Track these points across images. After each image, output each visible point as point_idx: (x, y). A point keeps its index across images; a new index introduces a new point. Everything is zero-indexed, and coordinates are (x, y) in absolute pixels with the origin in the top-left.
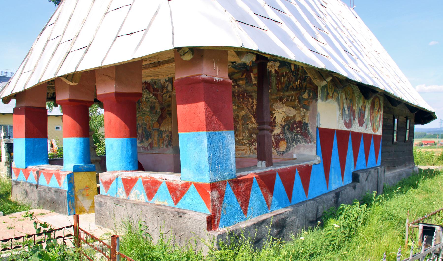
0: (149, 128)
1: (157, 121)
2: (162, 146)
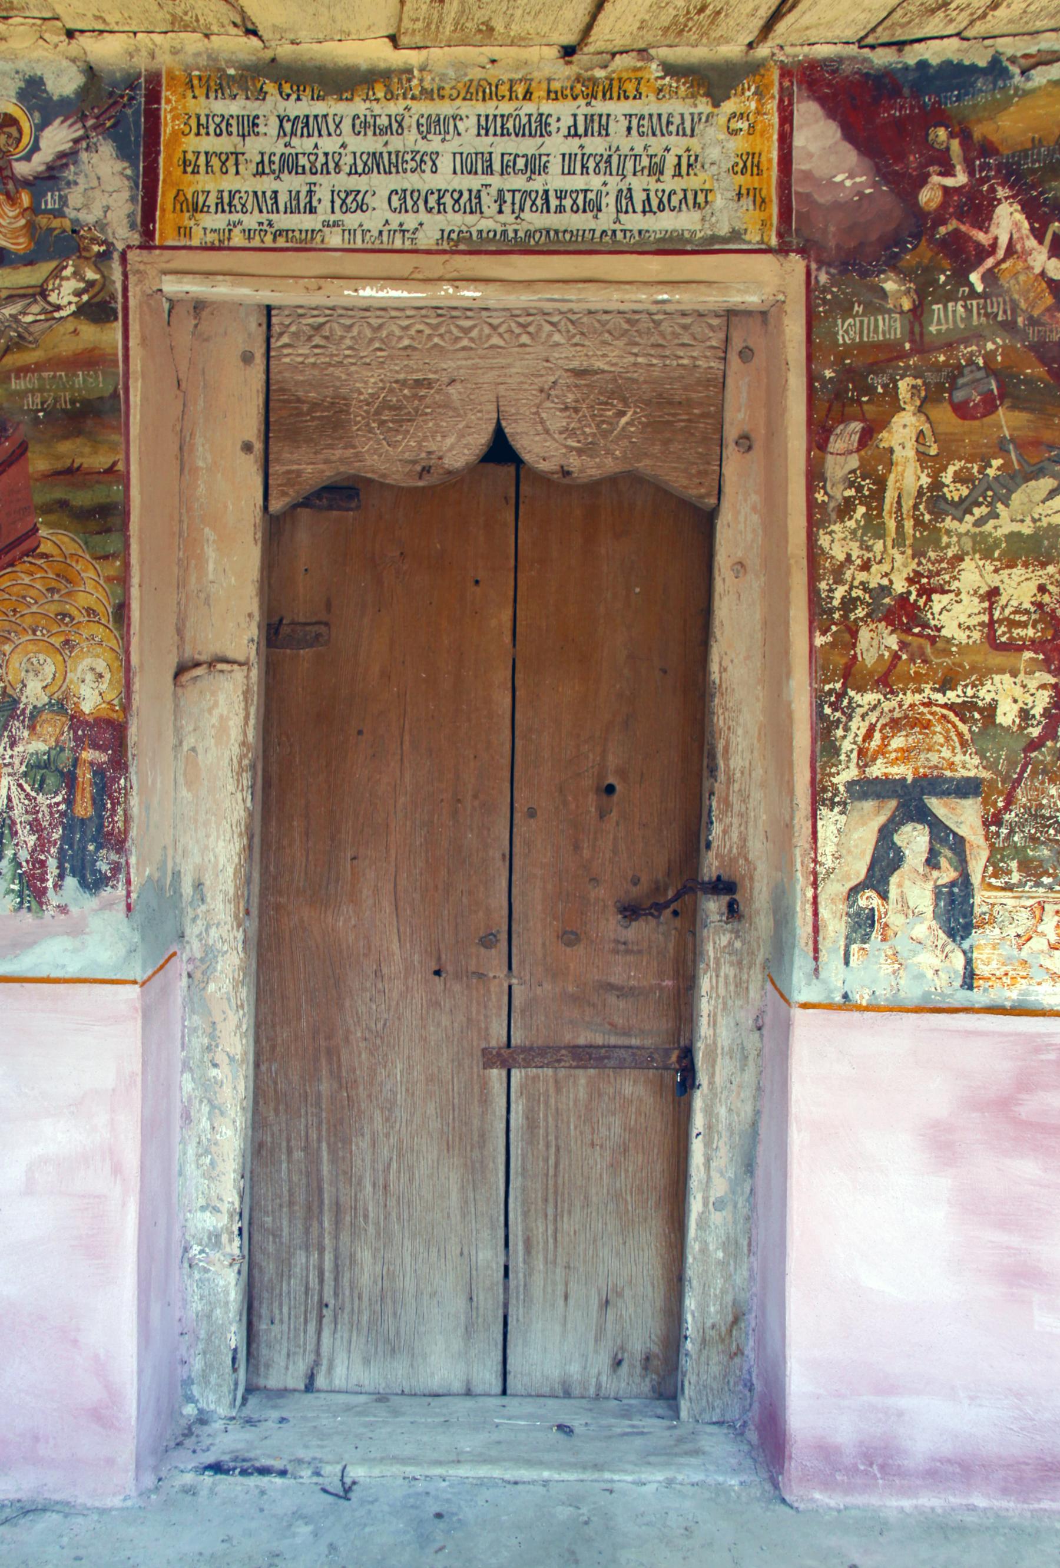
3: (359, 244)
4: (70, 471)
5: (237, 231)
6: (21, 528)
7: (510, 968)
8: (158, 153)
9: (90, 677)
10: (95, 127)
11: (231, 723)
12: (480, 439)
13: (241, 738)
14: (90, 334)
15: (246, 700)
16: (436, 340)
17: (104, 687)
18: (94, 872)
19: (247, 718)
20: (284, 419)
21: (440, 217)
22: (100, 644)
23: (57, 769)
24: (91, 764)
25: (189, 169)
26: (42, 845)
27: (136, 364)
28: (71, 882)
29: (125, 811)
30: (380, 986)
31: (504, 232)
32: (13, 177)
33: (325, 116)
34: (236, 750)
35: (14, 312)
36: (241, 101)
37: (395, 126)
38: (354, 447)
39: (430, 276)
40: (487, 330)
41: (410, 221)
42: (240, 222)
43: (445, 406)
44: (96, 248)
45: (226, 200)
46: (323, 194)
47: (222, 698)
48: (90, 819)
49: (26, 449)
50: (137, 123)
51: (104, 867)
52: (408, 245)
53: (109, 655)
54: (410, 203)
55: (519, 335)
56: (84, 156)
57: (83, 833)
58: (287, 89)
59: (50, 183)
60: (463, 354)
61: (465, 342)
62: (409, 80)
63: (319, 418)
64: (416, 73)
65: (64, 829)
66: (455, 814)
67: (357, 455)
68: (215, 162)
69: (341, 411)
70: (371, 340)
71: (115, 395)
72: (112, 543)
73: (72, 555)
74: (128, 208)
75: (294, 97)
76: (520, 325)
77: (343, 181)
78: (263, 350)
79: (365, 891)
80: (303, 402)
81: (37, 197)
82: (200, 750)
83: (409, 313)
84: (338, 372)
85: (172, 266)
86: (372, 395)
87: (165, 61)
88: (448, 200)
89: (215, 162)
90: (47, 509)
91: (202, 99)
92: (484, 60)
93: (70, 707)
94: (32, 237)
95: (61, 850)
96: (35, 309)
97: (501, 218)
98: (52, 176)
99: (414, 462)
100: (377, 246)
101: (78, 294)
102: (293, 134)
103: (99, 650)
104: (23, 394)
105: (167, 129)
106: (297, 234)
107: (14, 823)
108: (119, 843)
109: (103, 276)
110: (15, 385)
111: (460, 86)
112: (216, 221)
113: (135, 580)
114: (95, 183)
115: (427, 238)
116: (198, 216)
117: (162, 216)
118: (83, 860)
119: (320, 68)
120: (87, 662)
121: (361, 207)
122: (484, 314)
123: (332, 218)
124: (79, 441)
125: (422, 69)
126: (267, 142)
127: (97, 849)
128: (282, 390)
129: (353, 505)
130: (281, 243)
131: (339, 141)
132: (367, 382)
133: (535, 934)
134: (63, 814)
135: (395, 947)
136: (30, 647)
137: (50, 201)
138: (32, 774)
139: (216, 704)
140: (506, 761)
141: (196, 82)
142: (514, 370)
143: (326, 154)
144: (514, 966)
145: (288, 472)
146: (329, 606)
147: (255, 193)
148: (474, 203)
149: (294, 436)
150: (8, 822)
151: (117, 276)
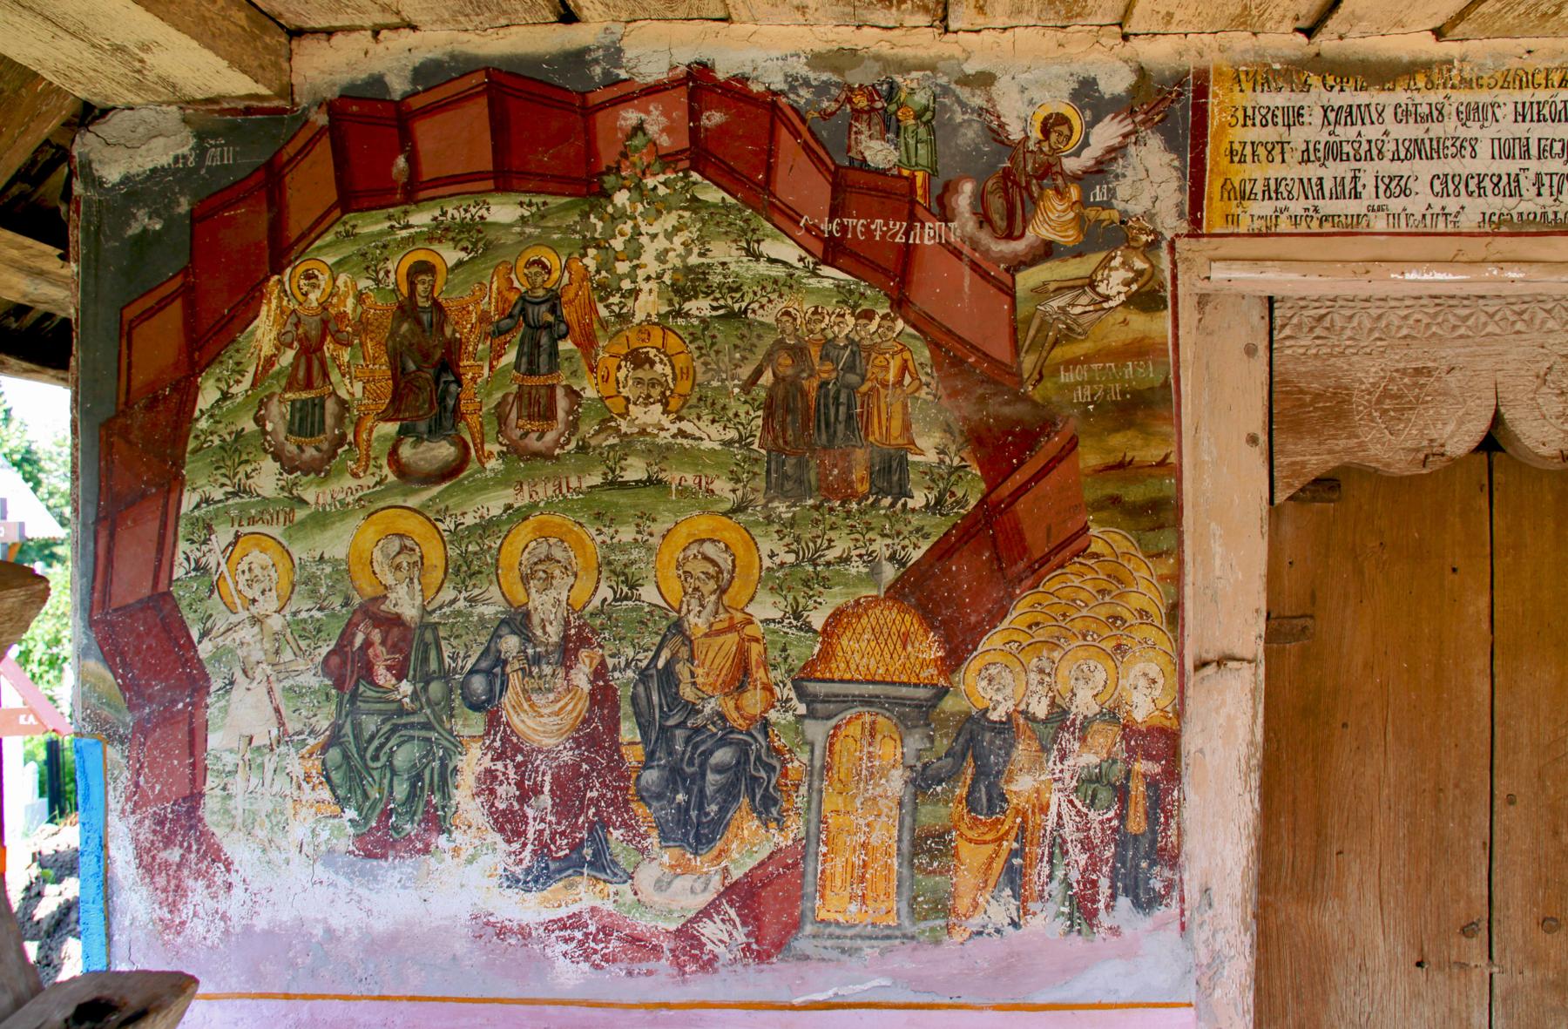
0: (740, 677)
1: (896, 592)
2: (999, 910)
3: (1403, 228)
4: (1121, 465)
5: (1283, 217)
6: (1072, 527)
7: (1490, 957)
8: (1205, 145)
9: (1142, 683)
10: (1143, 122)
11: (1239, 723)
12: (1478, 428)
13: (1249, 737)
14: (1140, 324)
15: (1254, 696)
16: (1434, 329)
17: (1156, 693)
18: (1148, 890)
19: (1255, 717)
20: (1288, 410)
21: (1481, 200)
22: (1153, 647)
23: (1109, 783)
24: (1144, 776)
25: (1236, 159)
26: (1093, 865)
27: (1186, 353)
28: (1124, 902)
29: (1178, 824)
30: (1364, 979)
31: (1544, 214)
32: (1062, 173)
33: (1368, 106)
34: (1243, 750)
35: (1062, 304)
36: (1286, 93)
37: (1435, 113)
38: (1357, 437)
39: (1474, 258)
40: (1483, 318)
41: (1452, 204)
42: (1287, 209)
43: (1445, 394)
44: (1144, 238)
45: (1273, 187)
46: (1367, 179)
47: (1229, 697)
48: (1143, 835)
49: (1076, 444)
50: (1185, 117)
51: (1157, 884)
52: (1450, 228)
53: (1163, 659)
54: (1451, 187)
55: (1514, 323)
56: (1132, 149)
57: (1136, 849)
58: (1330, 81)
59: (1099, 176)
60: (1461, 341)
61: (1462, 331)
62: (1449, 71)
63: (1322, 409)
64: (1456, 63)
65: (1116, 846)
66: (1436, 804)
67: (1360, 444)
68: (1261, 151)
69: (1344, 401)
70: (1371, 330)
71: (1166, 385)
72: (1165, 540)
73: (1124, 553)
74: (1177, 197)
75: (1337, 88)
76: (1515, 313)
77: (1387, 167)
78: (1266, 342)
79: (1350, 885)
80: (1306, 393)
81: (1086, 191)
82: (1207, 751)
83: (1407, 303)
84: (1340, 362)
85: (1221, 252)
86: (1373, 384)
87: (1212, 60)
88: (1487, 183)
89: (1261, 151)
90: (1098, 506)
91: (1249, 92)
92: (1521, 51)
93: (1122, 715)
94: (1081, 229)
95: (1114, 867)
96: (1084, 300)
97: (1540, 200)
98: (1100, 170)
99: (1418, 450)
100: (1421, 229)
101: (1127, 283)
102: (1337, 123)
103: (1151, 653)
104: (1071, 387)
105: (1216, 118)
106: (1343, 219)
107: (1064, 841)
108: (1171, 858)
109: (1152, 265)
110: (1064, 378)
111: (1498, 75)
112: (1264, 208)
113: (1189, 579)
114: (1143, 175)
115: (1469, 221)
116: (1246, 203)
117: (1210, 205)
118: (1136, 878)
119: (1362, 61)
120: (1139, 668)
121: (1404, 192)
122: (1481, 302)
123: (1377, 203)
124: (1130, 433)
125: (1462, 60)
126: (1313, 131)
127: (1151, 866)
128: (1285, 382)
129: (1335, 497)
130: (1327, 227)
131: (1382, 128)
132: (1367, 372)
133: (1515, 923)
134: (1115, 830)
135: (1380, 940)
136: (1081, 653)
137: (1099, 194)
138: (1083, 789)
139: (1223, 703)
140: (1486, 749)
141: (1243, 77)
142: (1510, 357)
143: (1369, 142)
144: (1495, 954)
145: (1293, 463)
146: (1313, 596)
147: (1301, 180)
148: (1513, 187)
149: (1297, 427)
150: (1059, 840)
151: (1165, 264)
